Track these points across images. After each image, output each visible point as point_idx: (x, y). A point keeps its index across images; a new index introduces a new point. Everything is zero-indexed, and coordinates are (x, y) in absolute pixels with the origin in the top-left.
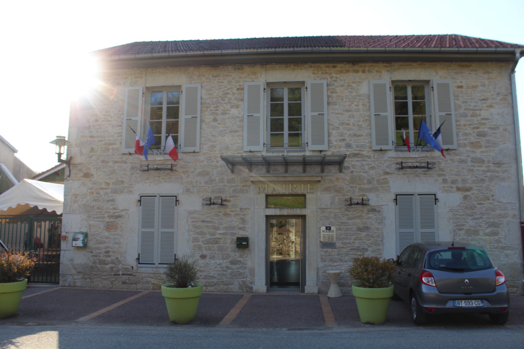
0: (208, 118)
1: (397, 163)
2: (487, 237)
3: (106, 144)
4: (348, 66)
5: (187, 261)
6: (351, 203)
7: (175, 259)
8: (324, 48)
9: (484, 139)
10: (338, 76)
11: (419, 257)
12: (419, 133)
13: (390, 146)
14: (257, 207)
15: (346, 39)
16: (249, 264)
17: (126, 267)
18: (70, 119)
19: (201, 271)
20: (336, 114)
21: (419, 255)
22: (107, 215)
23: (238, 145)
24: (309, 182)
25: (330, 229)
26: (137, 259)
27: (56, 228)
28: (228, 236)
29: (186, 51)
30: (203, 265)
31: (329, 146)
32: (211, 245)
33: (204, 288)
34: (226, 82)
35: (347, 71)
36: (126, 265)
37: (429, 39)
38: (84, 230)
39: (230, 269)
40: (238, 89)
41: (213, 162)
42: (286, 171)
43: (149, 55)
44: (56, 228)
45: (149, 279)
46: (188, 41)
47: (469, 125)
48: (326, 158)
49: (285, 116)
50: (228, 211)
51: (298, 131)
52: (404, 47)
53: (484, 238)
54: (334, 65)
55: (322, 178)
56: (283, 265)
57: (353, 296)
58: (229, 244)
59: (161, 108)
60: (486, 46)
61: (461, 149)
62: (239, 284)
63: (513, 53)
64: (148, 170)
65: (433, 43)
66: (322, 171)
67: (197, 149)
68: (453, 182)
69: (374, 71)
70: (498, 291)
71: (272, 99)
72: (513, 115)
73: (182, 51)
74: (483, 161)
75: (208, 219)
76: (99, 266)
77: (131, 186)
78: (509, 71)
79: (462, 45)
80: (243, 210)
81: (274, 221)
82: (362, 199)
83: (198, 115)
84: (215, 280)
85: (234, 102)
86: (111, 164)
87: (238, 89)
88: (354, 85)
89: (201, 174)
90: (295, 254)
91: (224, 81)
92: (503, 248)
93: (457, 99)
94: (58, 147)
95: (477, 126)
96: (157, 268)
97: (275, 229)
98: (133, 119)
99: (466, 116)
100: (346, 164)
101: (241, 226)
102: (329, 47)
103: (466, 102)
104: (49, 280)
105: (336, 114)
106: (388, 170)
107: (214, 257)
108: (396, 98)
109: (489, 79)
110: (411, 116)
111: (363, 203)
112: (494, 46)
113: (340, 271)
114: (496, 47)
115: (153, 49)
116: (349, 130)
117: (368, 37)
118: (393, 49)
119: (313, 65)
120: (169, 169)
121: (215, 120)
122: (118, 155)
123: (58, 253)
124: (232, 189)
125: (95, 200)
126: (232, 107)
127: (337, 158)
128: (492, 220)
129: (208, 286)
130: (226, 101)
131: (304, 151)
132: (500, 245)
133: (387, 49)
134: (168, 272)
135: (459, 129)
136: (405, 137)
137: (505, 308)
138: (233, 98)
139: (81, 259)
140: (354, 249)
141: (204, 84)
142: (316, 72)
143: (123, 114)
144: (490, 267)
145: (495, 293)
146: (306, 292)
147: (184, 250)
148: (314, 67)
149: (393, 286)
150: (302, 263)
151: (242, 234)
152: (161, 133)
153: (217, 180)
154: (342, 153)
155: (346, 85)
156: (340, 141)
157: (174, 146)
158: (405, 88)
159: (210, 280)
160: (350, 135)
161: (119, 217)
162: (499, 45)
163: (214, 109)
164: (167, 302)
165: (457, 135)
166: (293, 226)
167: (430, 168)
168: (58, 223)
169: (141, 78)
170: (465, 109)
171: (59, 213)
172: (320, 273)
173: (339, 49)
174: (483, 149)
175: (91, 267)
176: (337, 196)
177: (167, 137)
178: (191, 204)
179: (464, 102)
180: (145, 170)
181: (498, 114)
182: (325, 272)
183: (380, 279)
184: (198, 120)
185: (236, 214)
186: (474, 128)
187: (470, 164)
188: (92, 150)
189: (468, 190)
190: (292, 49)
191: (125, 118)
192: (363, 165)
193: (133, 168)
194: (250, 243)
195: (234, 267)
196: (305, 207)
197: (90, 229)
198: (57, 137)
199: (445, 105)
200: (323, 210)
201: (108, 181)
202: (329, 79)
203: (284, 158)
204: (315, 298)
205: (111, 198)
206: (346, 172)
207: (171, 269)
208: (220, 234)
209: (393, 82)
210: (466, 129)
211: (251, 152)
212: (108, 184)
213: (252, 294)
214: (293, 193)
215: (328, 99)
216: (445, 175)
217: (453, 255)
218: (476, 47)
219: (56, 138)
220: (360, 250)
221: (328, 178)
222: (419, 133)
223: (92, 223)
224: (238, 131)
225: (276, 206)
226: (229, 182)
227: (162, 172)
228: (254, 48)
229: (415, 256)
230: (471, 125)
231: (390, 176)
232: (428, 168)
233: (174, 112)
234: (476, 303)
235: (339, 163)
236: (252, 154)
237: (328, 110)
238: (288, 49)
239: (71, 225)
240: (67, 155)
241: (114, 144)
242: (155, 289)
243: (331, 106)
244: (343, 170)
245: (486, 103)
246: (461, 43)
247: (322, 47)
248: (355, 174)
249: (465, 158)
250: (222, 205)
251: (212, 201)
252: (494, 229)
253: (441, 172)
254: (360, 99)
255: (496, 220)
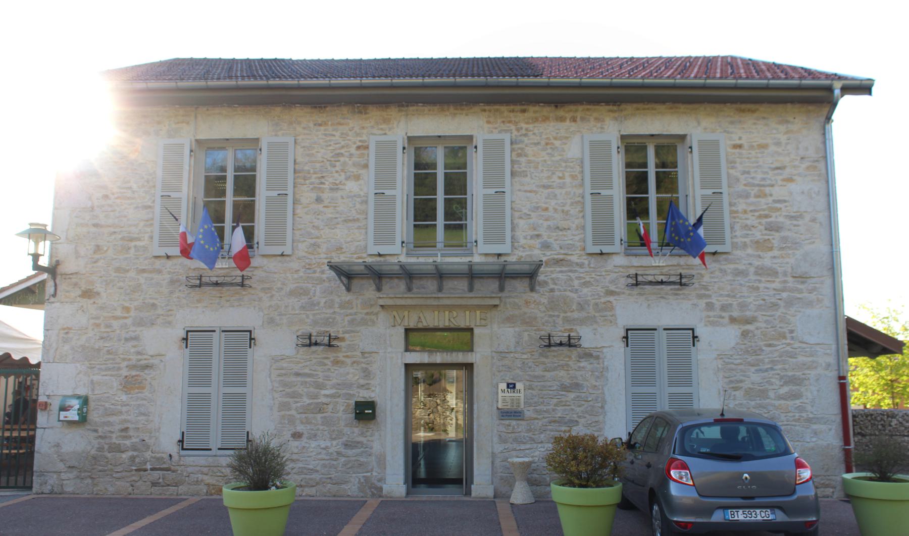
0: (307, 196)
1: (628, 276)
2: (782, 402)
3: (122, 239)
4: (546, 110)
5: (268, 444)
6: (549, 344)
7: (248, 441)
8: (507, 79)
9: (777, 235)
10: (531, 126)
11: (664, 436)
12: (666, 224)
13: (617, 247)
14: (389, 350)
15: (544, 63)
16: (376, 447)
17: (158, 455)
18: (56, 193)
19: (292, 460)
20: (526, 191)
21: (665, 432)
22: (125, 363)
23: (358, 244)
24: (479, 307)
25: (514, 387)
26: (179, 441)
27: (28, 388)
28: (339, 400)
29: (268, 79)
30: (296, 451)
31: (513, 246)
32: (311, 416)
33: (298, 490)
34: (338, 134)
35: (546, 119)
36: (158, 453)
37: (686, 64)
38: (82, 392)
39: (344, 456)
40: (358, 148)
41: (315, 272)
42: (440, 289)
43: (202, 83)
44: (28, 388)
45: (200, 476)
46: (270, 60)
47: (751, 211)
48: (508, 267)
49: (438, 195)
50: (341, 356)
51: (461, 220)
52: (643, 78)
53: (777, 403)
54: (524, 107)
55: (501, 301)
56: (435, 448)
57: (553, 501)
58: (343, 412)
59: (224, 178)
60: (783, 76)
61: (739, 253)
62: (359, 482)
63: (830, 89)
64: (200, 286)
65: (693, 70)
66: (502, 289)
67: (288, 251)
68: (724, 308)
69: (592, 119)
70: (801, 492)
71: (417, 166)
72: (828, 195)
73: (261, 79)
74: (775, 273)
75: (307, 371)
76: (109, 455)
77: (170, 313)
78: (823, 119)
79: (744, 75)
80: (366, 355)
81: (420, 374)
82: (569, 336)
83: (290, 192)
84: (316, 476)
85: (351, 170)
86: (132, 274)
87: (358, 148)
88: (557, 143)
89: (292, 293)
90: (456, 431)
91: (334, 133)
92: (809, 420)
93: (733, 168)
94: (32, 243)
95: (766, 212)
96: (215, 456)
97: (421, 387)
98: (173, 195)
99: (747, 196)
100: (541, 277)
101: (362, 382)
102: (516, 76)
103: (748, 173)
104: (12, 483)
105: (526, 191)
106: (612, 288)
107: (315, 435)
108: (628, 165)
109: (787, 133)
110: (653, 196)
111: (570, 343)
112: (797, 76)
113: (531, 459)
114: (801, 78)
115: (208, 72)
116: (547, 220)
117: (583, 59)
118: (624, 80)
119: (487, 108)
120: (237, 284)
121: (319, 200)
122: (146, 259)
123: (31, 433)
124: (347, 319)
125: (102, 338)
126: (347, 179)
127: (526, 268)
128: (790, 374)
129: (305, 486)
130: (337, 169)
131: (472, 254)
132: (804, 415)
133: (614, 80)
134: (235, 463)
135: (735, 218)
136: (642, 232)
137: (812, 523)
138: (350, 163)
139: (76, 443)
140: (554, 422)
141: (300, 138)
142: (492, 120)
143: (154, 186)
144: (787, 452)
145: (795, 497)
146: (473, 494)
147: (263, 424)
148: (490, 111)
149: (621, 484)
150: (467, 444)
151: (364, 395)
152: (223, 222)
153: (322, 304)
154: (535, 259)
155: (543, 143)
156: (532, 237)
157: (245, 244)
158: (643, 148)
159: (308, 477)
160: (549, 227)
161: (147, 367)
162: (806, 74)
163: (318, 181)
164: (232, 515)
165: (732, 228)
166: (453, 382)
167: (685, 285)
168: (31, 380)
169: (188, 123)
170: (745, 185)
171: (33, 361)
172: (498, 462)
173: (532, 80)
174: (776, 253)
175: (94, 458)
176: (526, 331)
177: (234, 228)
178: (276, 344)
179: (744, 173)
180: (196, 286)
181: (803, 193)
182: (505, 460)
183: (600, 472)
184: (290, 199)
185: (354, 362)
186: (760, 217)
187: (752, 277)
188: (98, 249)
189: (748, 321)
190: (451, 79)
191: (159, 193)
192: (571, 280)
193: (172, 282)
194: (378, 411)
195: (350, 452)
196: (472, 350)
197: (93, 390)
198: (31, 224)
199: (711, 175)
200: (502, 355)
201: (127, 305)
202: (515, 133)
203: (436, 266)
204: (488, 505)
205: (133, 335)
206: (541, 290)
207: (240, 458)
208: (326, 396)
209: (623, 137)
210: (746, 219)
211: (380, 255)
212: (127, 309)
213: (381, 499)
214: (452, 326)
215: (513, 167)
216: (709, 296)
217: (723, 432)
218: (766, 78)
219: (28, 227)
220: (566, 423)
221: (511, 300)
222: (666, 224)
223: (96, 378)
224: (358, 220)
225: (424, 348)
226: (342, 306)
227: (225, 288)
228: (386, 76)
229: (659, 434)
230: (755, 211)
231: (616, 297)
232: (681, 284)
233: (246, 184)
234: (763, 514)
235: (530, 275)
236: (382, 259)
237: (512, 185)
238: (445, 80)
239: (58, 384)
240: (51, 256)
241: (138, 239)
242: (211, 495)
243: (517, 179)
244: (537, 288)
245: (781, 174)
246: (742, 71)
247: (504, 76)
248: (557, 293)
249: (743, 267)
250: (330, 345)
251: (313, 339)
252: (794, 388)
253: (703, 292)
254: (566, 167)
255: (797, 374)
